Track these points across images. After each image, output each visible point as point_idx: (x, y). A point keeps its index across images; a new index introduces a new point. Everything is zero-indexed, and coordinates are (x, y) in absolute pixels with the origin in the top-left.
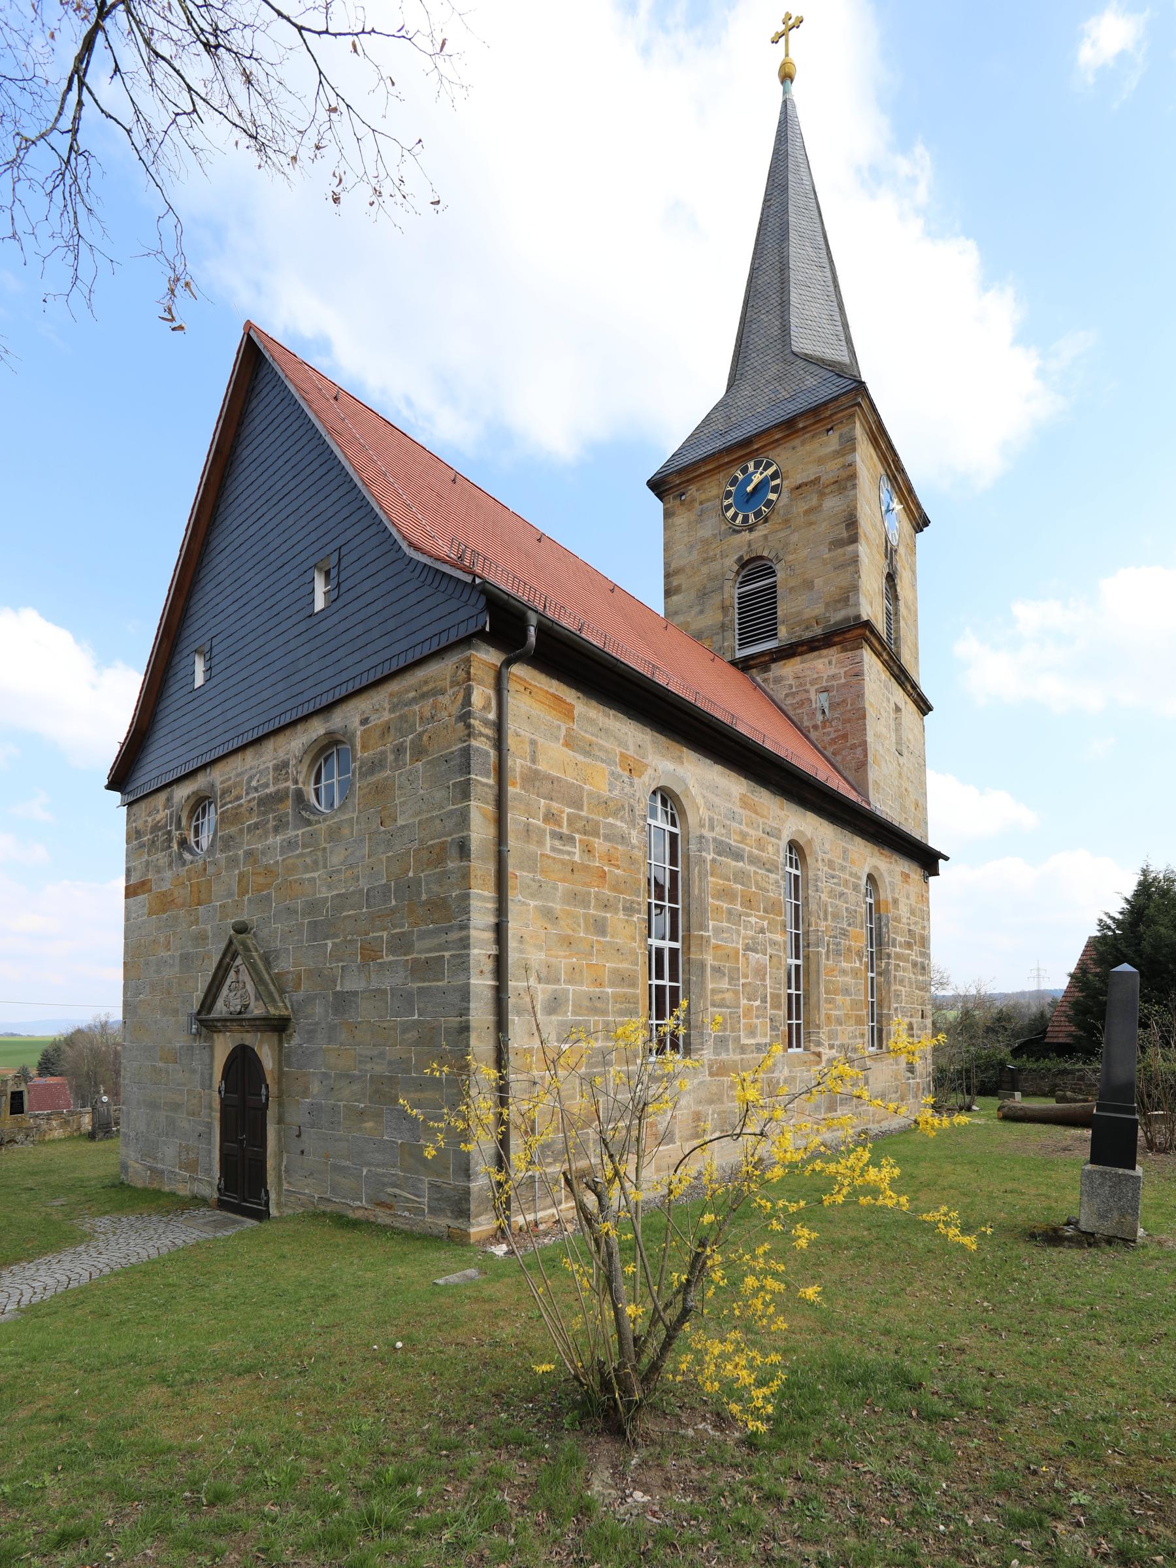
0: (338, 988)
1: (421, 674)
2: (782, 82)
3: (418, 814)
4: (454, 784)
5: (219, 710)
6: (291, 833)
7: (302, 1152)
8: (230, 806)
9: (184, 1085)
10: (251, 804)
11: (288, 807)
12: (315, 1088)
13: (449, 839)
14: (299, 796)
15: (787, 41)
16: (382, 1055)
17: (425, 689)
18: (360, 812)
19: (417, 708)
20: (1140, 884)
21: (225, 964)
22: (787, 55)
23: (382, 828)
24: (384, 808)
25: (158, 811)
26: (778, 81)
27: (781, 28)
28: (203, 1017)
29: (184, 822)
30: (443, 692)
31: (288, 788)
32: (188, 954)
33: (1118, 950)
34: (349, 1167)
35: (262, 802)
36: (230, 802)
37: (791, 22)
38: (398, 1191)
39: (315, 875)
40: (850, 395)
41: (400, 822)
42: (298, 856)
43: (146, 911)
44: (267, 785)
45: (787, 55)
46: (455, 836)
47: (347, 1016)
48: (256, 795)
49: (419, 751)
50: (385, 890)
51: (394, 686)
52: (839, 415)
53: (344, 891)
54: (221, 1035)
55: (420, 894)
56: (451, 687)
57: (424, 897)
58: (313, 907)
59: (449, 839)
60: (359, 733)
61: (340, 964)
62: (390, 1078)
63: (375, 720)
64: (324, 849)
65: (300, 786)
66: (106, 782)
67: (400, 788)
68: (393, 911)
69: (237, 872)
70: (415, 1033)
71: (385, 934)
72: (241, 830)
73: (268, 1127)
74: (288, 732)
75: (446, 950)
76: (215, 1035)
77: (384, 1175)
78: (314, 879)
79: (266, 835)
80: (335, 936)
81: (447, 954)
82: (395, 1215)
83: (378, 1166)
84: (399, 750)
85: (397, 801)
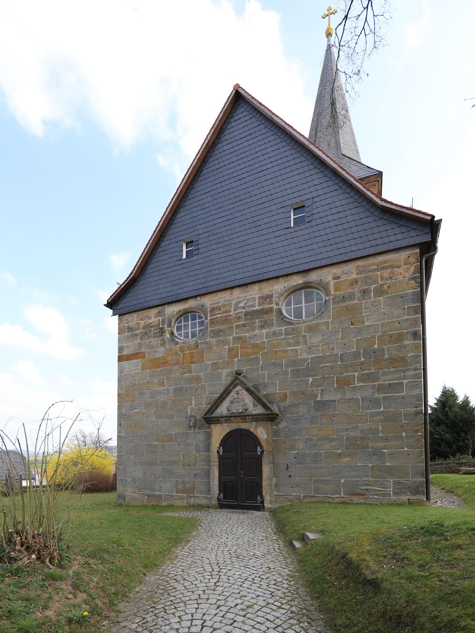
0: (319, 399)
1: (381, 258)
2: (327, 37)
3: (380, 320)
4: (408, 308)
5: (193, 268)
6: (275, 328)
7: (290, 476)
8: (219, 315)
9: (181, 452)
10: (240, 315)
11: (274, 317)
12: (301, 445)
13: (405, 331)
14: (280, 312)
15: (329, 19)
16: (356, 428)
17: (385, 265)
18: (333, 319)
19: (379, 273)
20: (443, 392)
21: (229, 389)
22: (329, 25)
23: (352, 326)
24: (354, 317)
25: (133, 319)
26: (325, 36)
27: (327, 13)
28: (208, 416)
29: (172, 324)
30: (398, 267)
31: (272, 308)
32: (182, 388)
33: (438, 417)
34: (330, 480)
35: (247, 314)
36: (220, 314)
37: (331, 11)
38: (369, 487)
39: (298, 348)
40: (375, 176)
41: (366, 324)
42: (282, 339)
43: (139, 367)
44: (254, 306)
45: (329, 25)
46: (409, 330)
47: (326, 412)
48: (244, 311)
49: (380, 292)
50: (356, 355)
51: (360, 263)
52: (369, 184)
53: (321, 355)
54: (218, 426)
55: (384, 355)
56: (404, 265)
57: (386, 357)
58: (295, 362)
59: (405, 331)
60: (332, 283)
61: (320, 388)
62: (362, 438)
63: (343, 278)
64: (305, 336)
65: (280, 307)
66: (106, 303)
67: (366, 308)
68: (362, 363)
69: (227, 347)
70: (382, 417)
71: (356, 374)
72: (231, 328)
73: (264, 466)
74: (275, 280)
75: (405, 379)
76: (213, 426)
77: (357, 481)
78: (297, 350)
79: (253, 329)
80: (315, 375)
81: (405, 381)
82: (367, 498)
83: (353, 477)
84: (365, 292)
85: (364, 314)
